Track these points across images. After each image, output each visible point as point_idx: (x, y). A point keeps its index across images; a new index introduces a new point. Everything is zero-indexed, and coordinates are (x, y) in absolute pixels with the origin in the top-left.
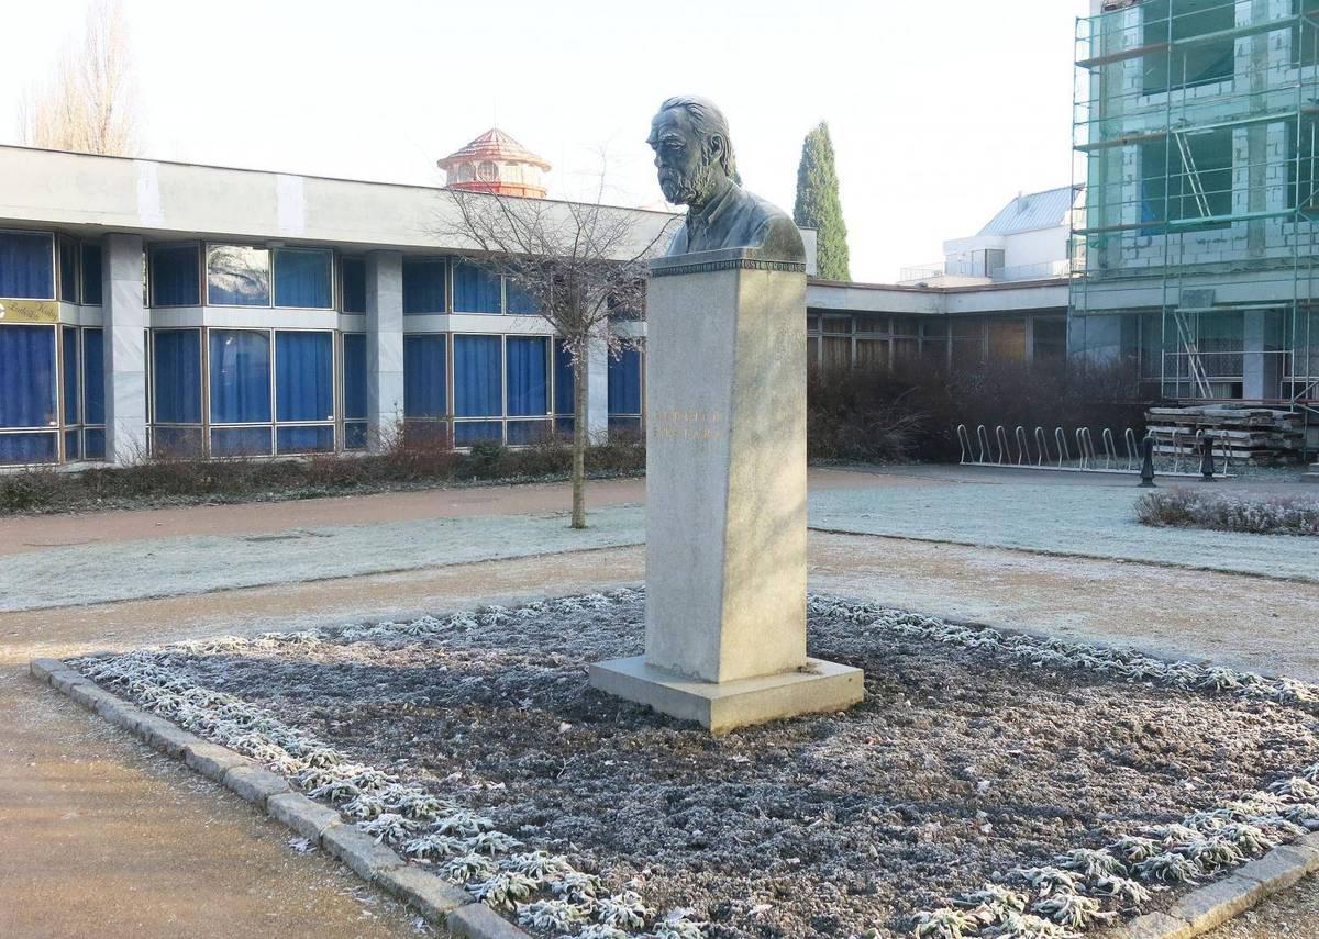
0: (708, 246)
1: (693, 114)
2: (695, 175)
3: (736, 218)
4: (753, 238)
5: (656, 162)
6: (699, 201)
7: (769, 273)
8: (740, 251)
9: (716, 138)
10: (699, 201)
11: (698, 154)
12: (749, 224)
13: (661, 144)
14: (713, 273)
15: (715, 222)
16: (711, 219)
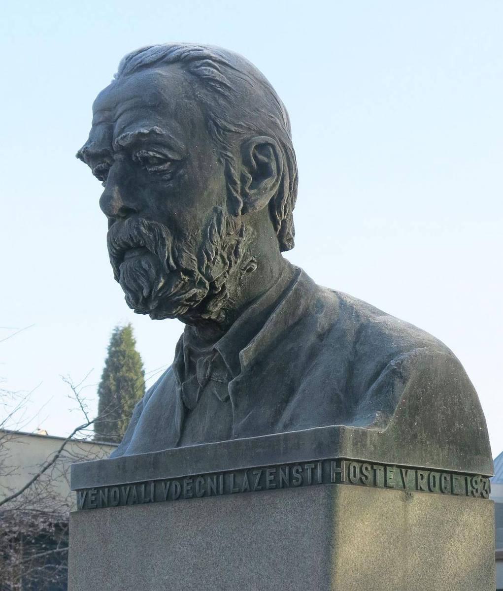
0: (237, 426)
1: (206, 82)
2: (207, 237)
3: (313, 354)
4: (366, 402)
5: (105, 203)
6: (216, 310)
7: (408, 497)
8: (335, 437)
9: (262, 147)
10: (216, 310)
11: (217, 185)
12: (351, 368)
13: (119, 156)
14: (255, 499)
15: (258, 364)
16: (246, 355)
